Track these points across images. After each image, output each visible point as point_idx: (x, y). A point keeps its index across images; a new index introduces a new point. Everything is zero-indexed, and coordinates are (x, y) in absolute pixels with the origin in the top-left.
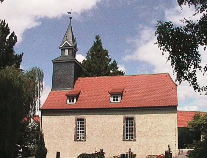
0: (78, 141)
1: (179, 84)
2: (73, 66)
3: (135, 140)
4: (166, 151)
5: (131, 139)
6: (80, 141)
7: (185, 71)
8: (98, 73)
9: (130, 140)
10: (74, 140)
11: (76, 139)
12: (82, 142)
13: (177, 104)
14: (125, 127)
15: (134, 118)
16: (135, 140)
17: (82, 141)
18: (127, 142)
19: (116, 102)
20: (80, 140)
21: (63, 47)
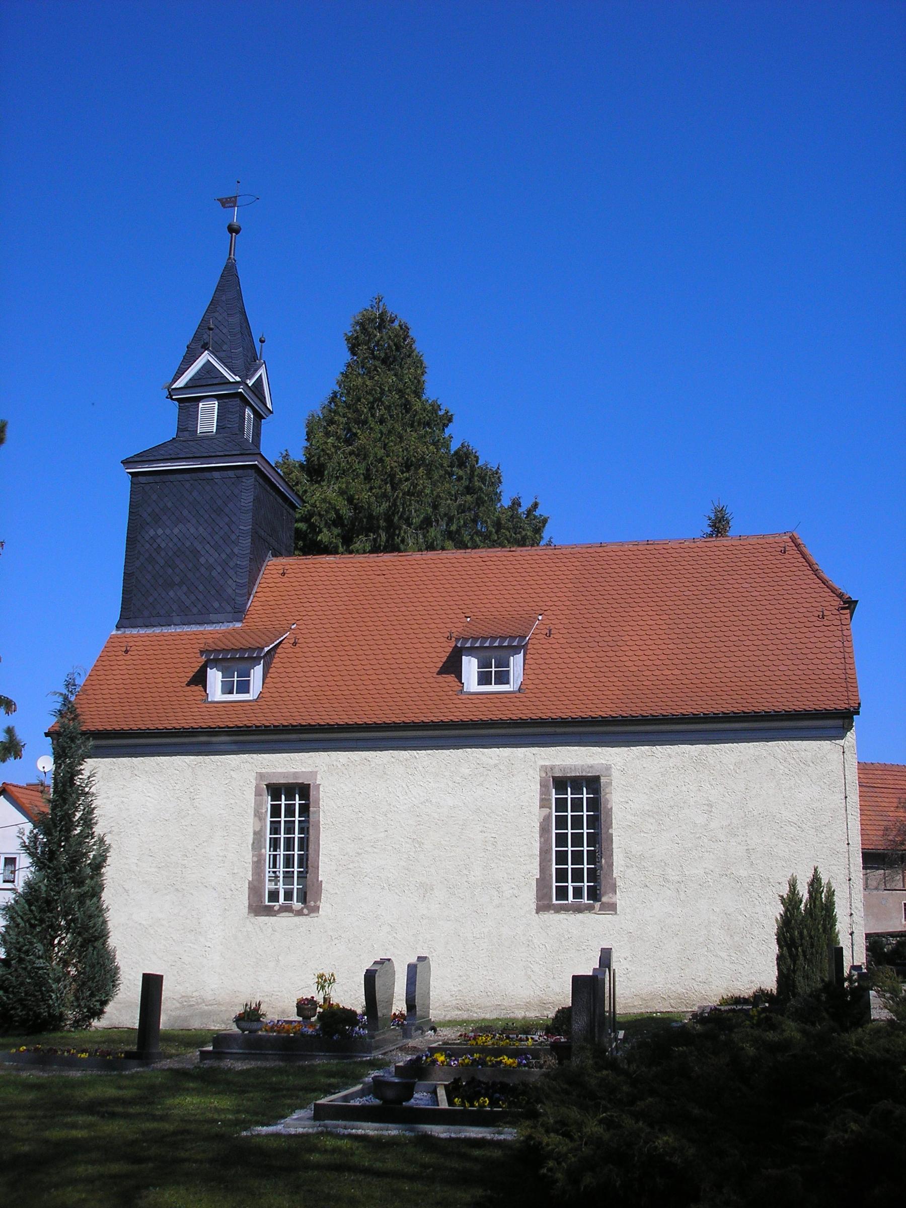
0: (269, 911)
1: (332, 975)
2: (248, 493)
3: (612, 908)
4: (791, 902)
5: (585, 900)
6: (286, 914)
7: (488, 1059)
8: (370, 529)
9: (578, 909)
10: (250, 906)
11: (263, 905)
12: (297, 919)
13: (849, 682)
14: (550, 831)
15: (603, 780)
16: (612, 908)
17: (299, 913)
18: (562, 916)
19: (493, 688)
20: (286, 909)
21: (186, 387)
